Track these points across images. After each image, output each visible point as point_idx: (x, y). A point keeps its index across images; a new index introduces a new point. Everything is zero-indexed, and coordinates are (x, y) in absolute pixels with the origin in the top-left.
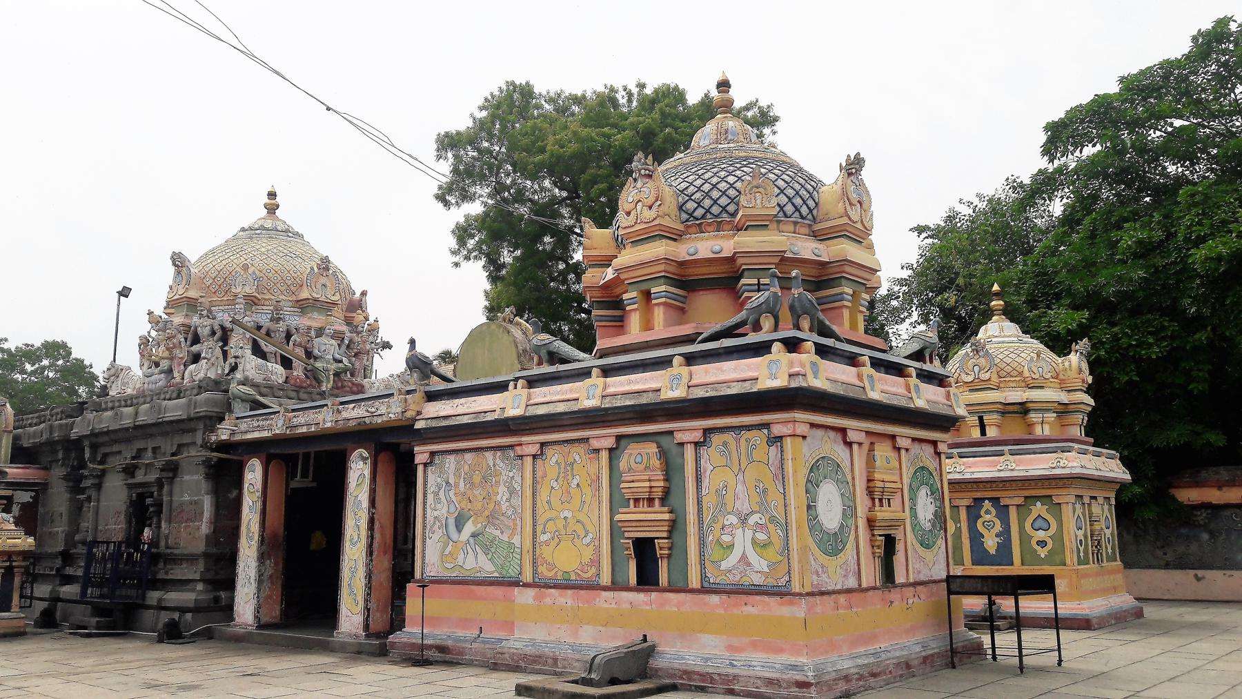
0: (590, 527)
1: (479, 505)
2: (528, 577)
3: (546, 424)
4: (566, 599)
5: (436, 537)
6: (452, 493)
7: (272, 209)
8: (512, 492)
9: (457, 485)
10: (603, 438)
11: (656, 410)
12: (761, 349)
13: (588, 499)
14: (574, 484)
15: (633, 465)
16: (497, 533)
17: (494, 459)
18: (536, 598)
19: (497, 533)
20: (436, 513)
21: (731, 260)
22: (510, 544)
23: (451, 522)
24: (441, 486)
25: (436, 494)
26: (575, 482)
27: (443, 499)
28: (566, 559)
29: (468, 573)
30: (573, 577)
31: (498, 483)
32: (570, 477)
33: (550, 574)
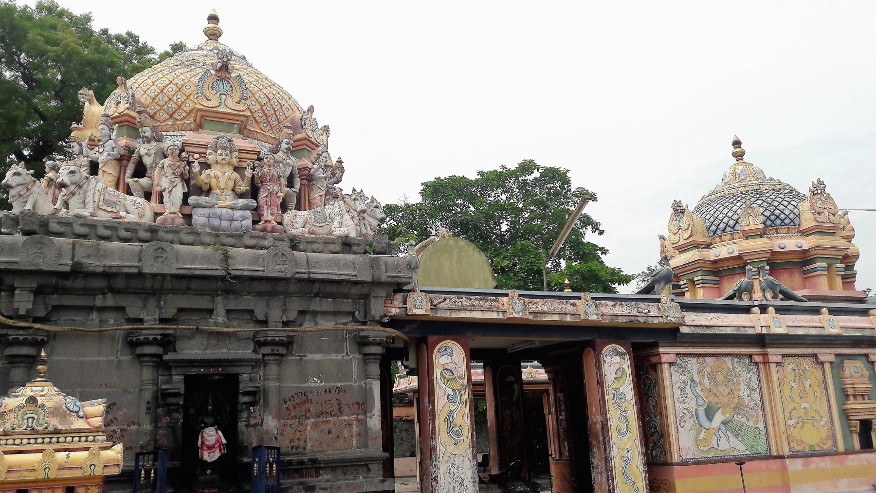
0: (822, 414)
1: (726, 400)
2: (787, 452)
3: (792, 342)
4: (826, 463)
5: (688, 426)
6: (698, 389)
7: (739, 156)
8: (751, 389)
9: (702, 383)
10: (827, 355)
11: (863, 340)
12: (747, 310)
13: (819, 395)
14: (807, 385)
15: (854, 374)
16: (744, 420)
17: (733, 363)
18: (804, 465)
19: (744, 420)
20: (685, 406)
21: (739, 257)
22: (756, 429)
23: (702, 412)
24: (683, 382)
25: (682, 390)
26: (808, 383)
27: (690, 394)
28: (813, 436)
29: (723, 454)
30: (817, 448)
31: (738, 382)
32: (803, 379)
33: (800, 448)
